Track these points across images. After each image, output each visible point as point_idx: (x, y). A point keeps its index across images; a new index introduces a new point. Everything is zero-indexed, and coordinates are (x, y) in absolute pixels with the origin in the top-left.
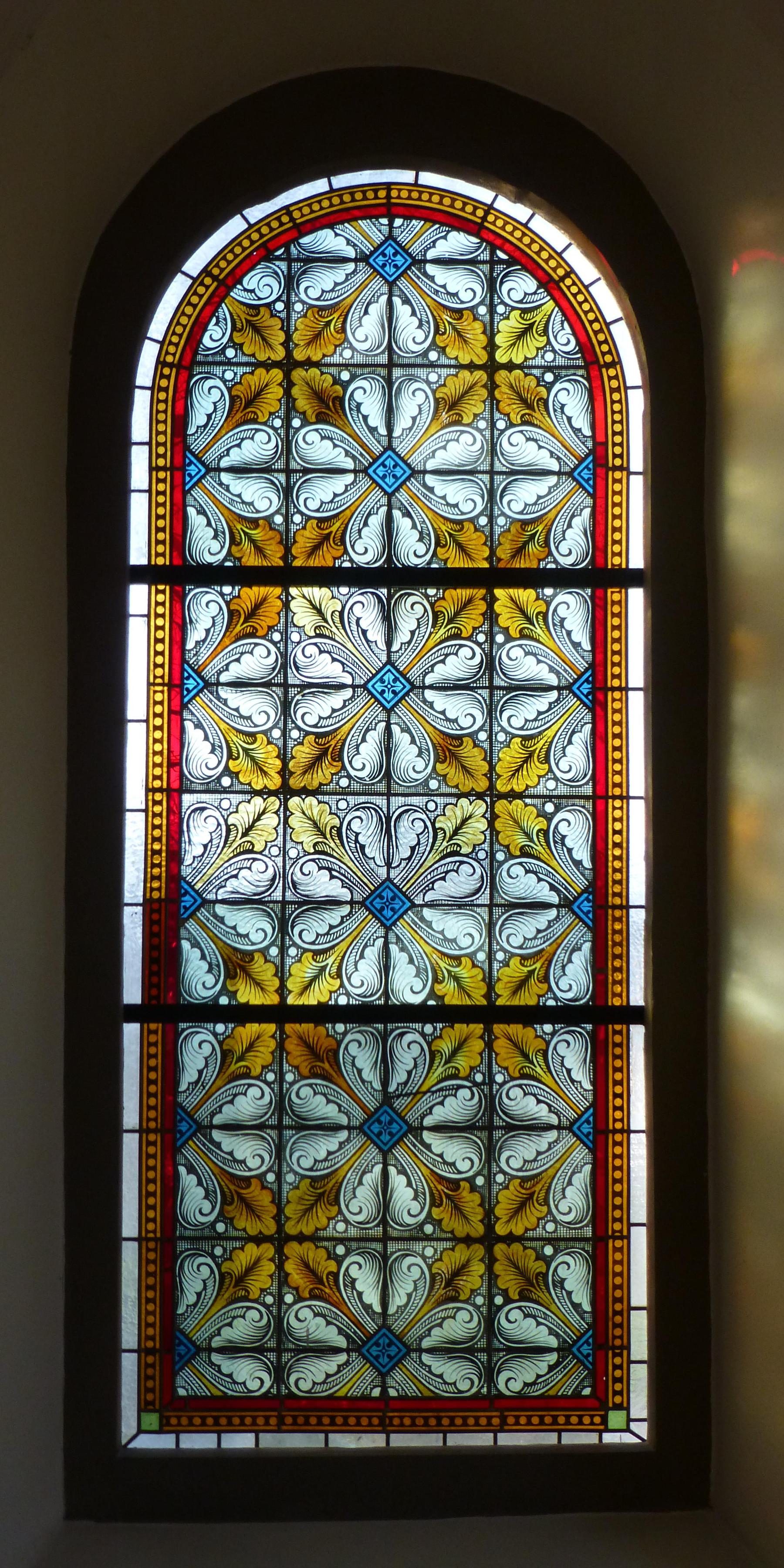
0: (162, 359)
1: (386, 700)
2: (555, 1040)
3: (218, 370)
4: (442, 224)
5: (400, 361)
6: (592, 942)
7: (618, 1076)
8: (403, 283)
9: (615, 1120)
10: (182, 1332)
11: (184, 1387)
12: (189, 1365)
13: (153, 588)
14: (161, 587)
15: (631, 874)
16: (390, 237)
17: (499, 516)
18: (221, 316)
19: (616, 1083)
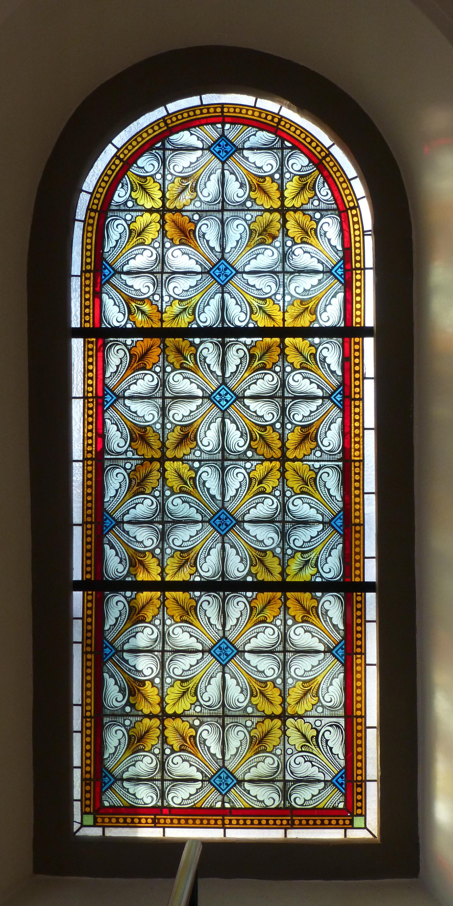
0: (90, 207)
1: (222, 659)
2: (321, 472)
3: (122, 214)
4: (253, 127)
5: (230, 713)
6: (344, 673)
7: (359, 750)
8: (231, 411)
9: (355, 393)
10: (107, 769)
11: (107, 801)
12: (112, 531)
13: (86, 592)
14: (90, 592)
15: (365, 408)
16: (223, 136)
17: (286, 172)
18: (125, 182)
19: (358, 753)
